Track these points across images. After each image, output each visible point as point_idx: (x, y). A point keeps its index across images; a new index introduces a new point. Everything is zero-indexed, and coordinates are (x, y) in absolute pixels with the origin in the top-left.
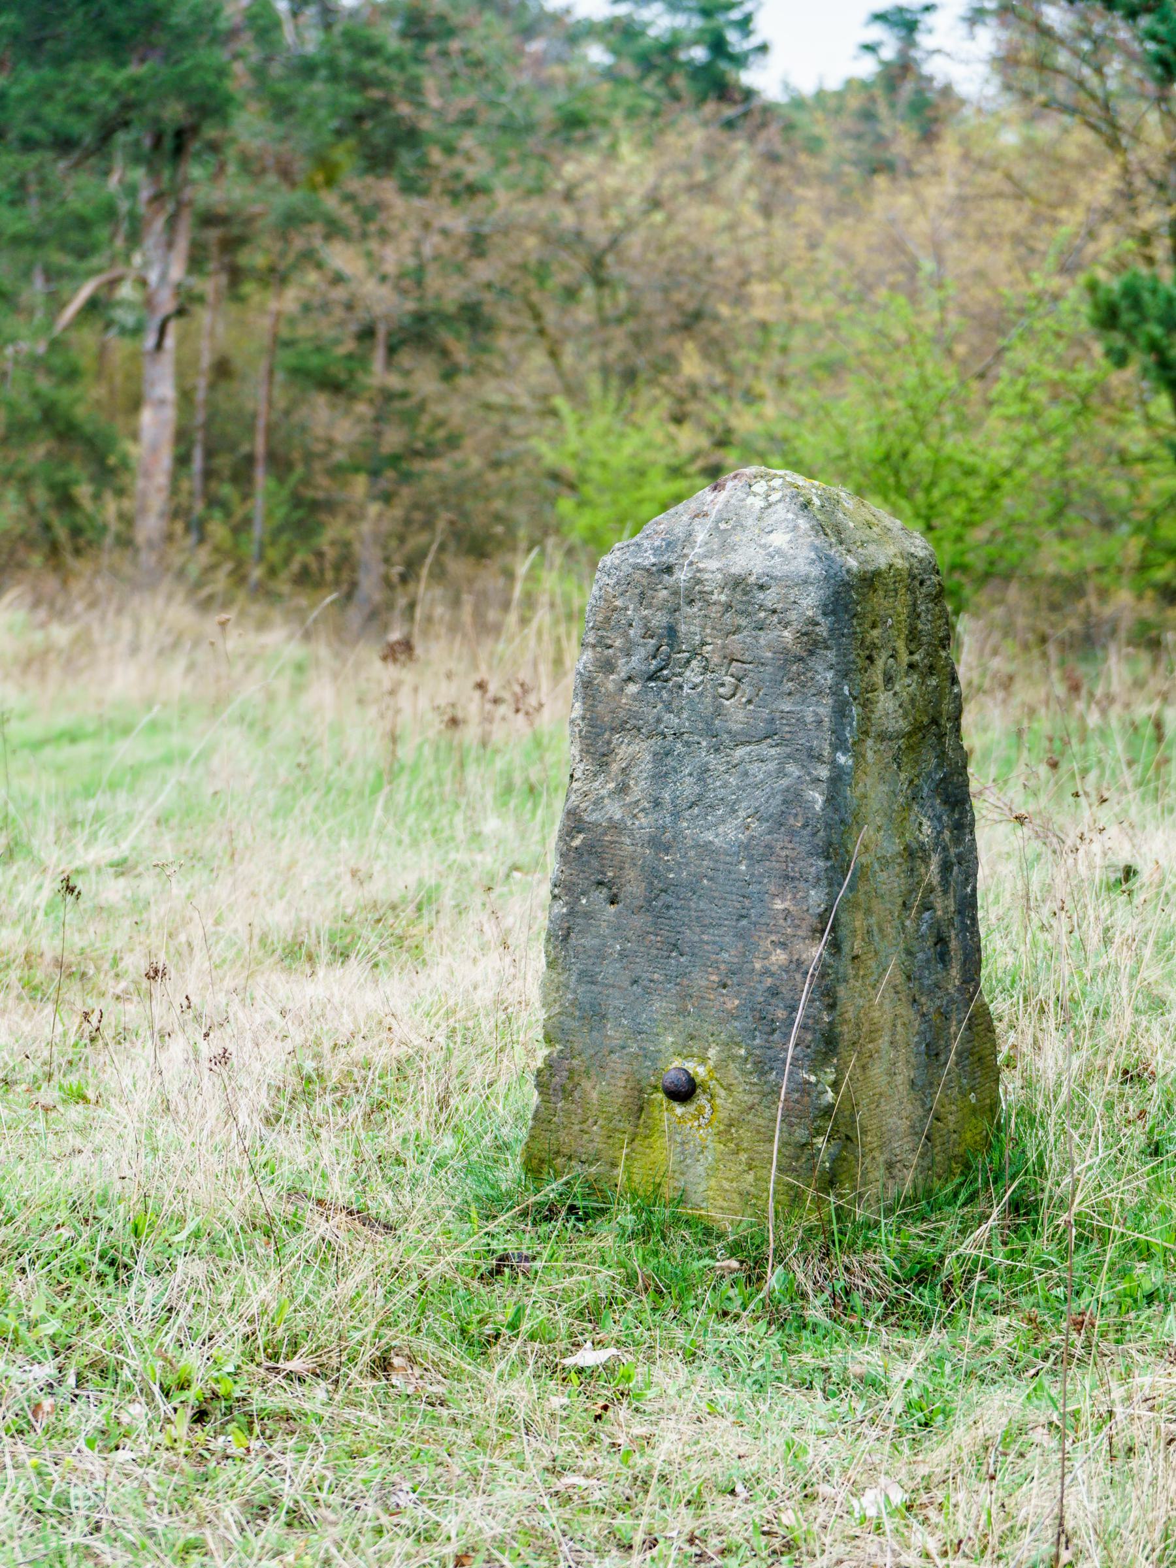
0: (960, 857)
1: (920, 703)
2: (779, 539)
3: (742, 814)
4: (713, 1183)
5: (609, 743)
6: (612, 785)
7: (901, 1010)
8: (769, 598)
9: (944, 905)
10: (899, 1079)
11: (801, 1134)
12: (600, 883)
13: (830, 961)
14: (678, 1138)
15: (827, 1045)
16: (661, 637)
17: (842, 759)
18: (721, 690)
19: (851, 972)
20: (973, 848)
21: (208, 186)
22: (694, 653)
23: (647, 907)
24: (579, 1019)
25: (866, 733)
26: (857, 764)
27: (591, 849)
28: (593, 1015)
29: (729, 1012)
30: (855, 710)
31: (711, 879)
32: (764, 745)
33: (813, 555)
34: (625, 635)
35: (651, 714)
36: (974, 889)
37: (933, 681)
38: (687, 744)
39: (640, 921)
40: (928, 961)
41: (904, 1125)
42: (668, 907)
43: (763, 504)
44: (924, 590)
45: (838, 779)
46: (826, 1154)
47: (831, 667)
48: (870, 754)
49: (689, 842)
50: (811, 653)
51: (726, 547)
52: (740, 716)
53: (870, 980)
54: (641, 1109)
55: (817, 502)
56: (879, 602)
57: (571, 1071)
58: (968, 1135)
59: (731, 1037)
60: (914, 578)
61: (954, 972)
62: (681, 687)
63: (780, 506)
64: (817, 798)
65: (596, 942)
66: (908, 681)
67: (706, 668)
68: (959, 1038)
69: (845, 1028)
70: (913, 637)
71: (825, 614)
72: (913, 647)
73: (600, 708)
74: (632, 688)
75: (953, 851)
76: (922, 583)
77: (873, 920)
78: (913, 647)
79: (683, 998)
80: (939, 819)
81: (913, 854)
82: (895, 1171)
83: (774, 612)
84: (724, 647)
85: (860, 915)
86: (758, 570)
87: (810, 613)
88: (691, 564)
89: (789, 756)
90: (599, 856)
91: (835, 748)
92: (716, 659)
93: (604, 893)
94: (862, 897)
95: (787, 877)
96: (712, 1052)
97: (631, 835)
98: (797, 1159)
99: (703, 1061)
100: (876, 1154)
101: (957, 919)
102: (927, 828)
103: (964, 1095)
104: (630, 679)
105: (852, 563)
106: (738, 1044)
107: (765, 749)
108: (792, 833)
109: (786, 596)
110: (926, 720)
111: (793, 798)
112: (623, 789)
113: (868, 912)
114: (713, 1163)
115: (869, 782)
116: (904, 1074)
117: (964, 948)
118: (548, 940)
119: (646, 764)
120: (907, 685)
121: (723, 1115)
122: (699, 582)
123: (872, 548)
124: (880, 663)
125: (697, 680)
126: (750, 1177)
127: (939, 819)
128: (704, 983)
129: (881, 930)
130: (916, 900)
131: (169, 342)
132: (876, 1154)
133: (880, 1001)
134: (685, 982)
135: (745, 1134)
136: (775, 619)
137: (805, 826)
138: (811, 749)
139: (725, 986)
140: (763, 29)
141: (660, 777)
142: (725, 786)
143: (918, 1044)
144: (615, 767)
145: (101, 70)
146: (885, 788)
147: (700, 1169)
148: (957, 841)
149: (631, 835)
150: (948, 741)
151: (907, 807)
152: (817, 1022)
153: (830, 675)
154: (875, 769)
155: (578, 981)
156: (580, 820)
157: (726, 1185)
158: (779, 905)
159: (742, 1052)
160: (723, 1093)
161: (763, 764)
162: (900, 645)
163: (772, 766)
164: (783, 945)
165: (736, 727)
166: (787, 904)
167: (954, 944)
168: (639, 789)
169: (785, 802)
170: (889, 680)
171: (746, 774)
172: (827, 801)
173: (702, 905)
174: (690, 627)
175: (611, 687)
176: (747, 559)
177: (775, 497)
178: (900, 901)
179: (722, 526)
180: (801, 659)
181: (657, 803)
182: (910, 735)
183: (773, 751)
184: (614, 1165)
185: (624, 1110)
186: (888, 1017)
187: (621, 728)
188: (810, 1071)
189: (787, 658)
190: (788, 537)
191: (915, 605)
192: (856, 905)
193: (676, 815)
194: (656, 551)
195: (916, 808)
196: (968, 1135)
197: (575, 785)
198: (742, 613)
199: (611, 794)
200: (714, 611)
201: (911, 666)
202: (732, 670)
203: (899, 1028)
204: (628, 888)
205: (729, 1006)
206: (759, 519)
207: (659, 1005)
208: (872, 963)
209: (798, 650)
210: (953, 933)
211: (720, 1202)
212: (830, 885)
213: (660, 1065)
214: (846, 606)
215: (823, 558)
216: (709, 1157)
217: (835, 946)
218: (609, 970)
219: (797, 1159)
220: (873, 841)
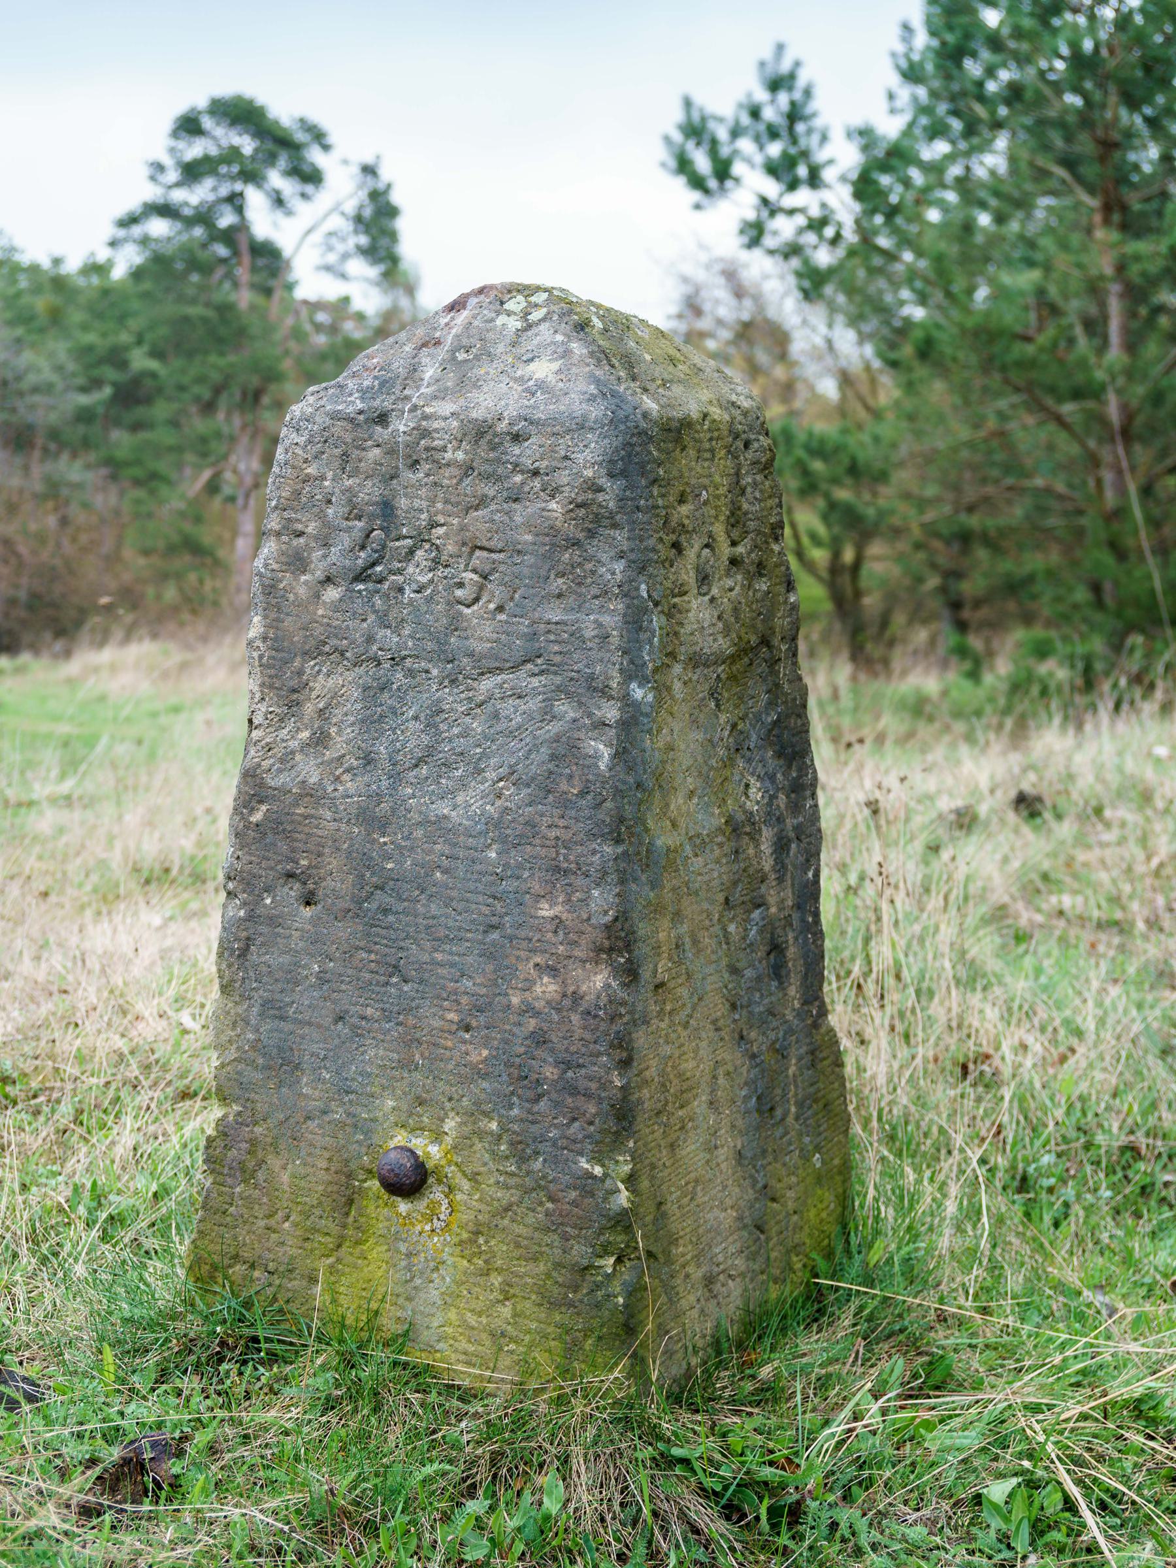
0: (798, 829)
1: (746, 614)
2: (543, 369)
3: (491, 775)
4: (452, 1315)
5: (300, 673)
6: (305, 735)
7: (725, 1055)
8: (528, 453)
9: (779, 898)
10: (722, 1153)
11: (579, 1252)
12: (290, 875)
13: (622, 994)
14: (403, 1247)
16: (372, 517)
17: (638, 693)
18: (459, 593)
19: (654, 1008)
20: (815, 817)
22: (420, 539)
23: (355, 911)
24: (265, 1060)
25: (672, 655)
26: (659, 700)
27: (276, 826)
28: (282, 1063)
29: (474, 1067)
30: (657, 621)
31: (445, 872)
32: (522, 674)
33: (592, 389)
34: (321, 516)
35: (359, 630)
36: (817, 874)
37: (762, 585)
38: (411, 673)
39: (344, 931)
40: (759, 979)
41: (727, 1218)
42: (386, 911)
43: (519, 325)
44: (750, 455)
45: (632, 723)
47: (621, 556)
48: (677, 686)
49: (415, 817)
50: (592, 534)
51: (465, 383)
52: (487, 629)
53: (682, 1016)
54: (350, 1202)
55: (598, 323)
56: (687, 465)
57: (253, 1142)
58: (812, 1213)
59: (477, 1103)
60: (737, 437)
61: (792, 991)
62: (401, 590)
63: (543, 327)
64: (602, 751)
65: (286, 959)
66: (730, 583)
67: (436, 562)
68: (796, 1082)
69: (646, 1093)
70: (736, 519)
71: (611, 475)
72: (735, 534)
73: (288, 622)
74: (332, 594)
75: (790, 822)
76: (747, 445)
77: (684, 928)
78: (735, 534)
79: (408, 1044)
80: (772, 778)
81: (738, 829)
82: (717, 1287)
83: (536, 473)
84: (463, 528)
85: (666, 923)
86: (511, 412)
87: (589, 473)
88: (415, 408)
89: (558, 689)
90: (288, 836)
91: (628, 676)
92: (451, 548)
93: (293, 891)
94: (668, 896)
95: (557, 869)
96: (450, 1125)
97: (333, 807)
98: (576, 1289)
99: (438, 1136)
100: (690, 1269)
101: (796, 916)
102: (755, 793)
103: (806, 1157)
104: (328, 580)
105: (650, 404)
106: (486, 1114)
107: (524, 679)
108: (565, 803)
109: (553, 449)
110: (754, 640)
111: (566, 751)
112: (320, 740)
113: (677, 916)
115: (677, 726)
116: (728, 1143)
117: (805, 956)
118: (220, 955)
119: (351, 706)
121: (466, 1217)
122: (426, 434)
123: (677, 390)
124: (691, 554)
125: (424, 579)
126: (506, 1311)
127: (772, 778)
128: (437, 1023)
129: (695, 942)
130: (743, 896)
131: (252, 502)
132: (690, 1269)
133: (696, 1055)
134: (411, 1021)
135: (499, 1247)
136: (537, 484)
137: (583, 793)
138: (592, 677)
139: (467, 1029)
141: (371, 722)
142: (464, 734)
143: (746, 1098)
144: (309, 709)
145: (213, 358)
146: (700, 736)
147: (434, 1294)
148: (795, 807)
149: (333, 807)
150: (783, 670)
151: (728, 763)
152: (603, 1087)
153: (619, 566)
154: (685, 708)
155: (261, 1014)
156: (262, 785)
157: (472, 1320)
158: (546, 911)
159: (494, 1126)
160: (466, 1185)
161: (521, 703)
162: (719, 529)
163: (534, 704)
164: (553, 971)
165: (480, 647)
166: (558, 910)
167: (792, 952)
168: (342, 741)
169: (553, 757)
170: (704, 579)
171: (496, 716)
172: (616, 756)
173: (434, 909)
174: (414, 499)
175: (302, 591)
177: (536, 315)
178: (721, 897)
179: (461, 356)
180: (577, 543)
181: (368, 760)
182: (733, 659)
183: (535, 682)
184: (313, 1280)
185: (327, 1202)
186: (707, 1066)
187: (316, 651)
188: (593, 1160)
189: (556, 541)
190: (555, 366)
191: (737, 474)
192: (658, 909)
193: (396, 777)
194: (364, 392)
195: (741, 764)
196: (812, 1213)
197: (256, 734)
198: (486, 477)
199: (305, 746)
200: (447, 477)
201: (734, 562)
202: (475, 562)
203: (721, 1081)
204: (329, 882)
205: (474, 1058)
206: (514, 344)
207: (374, 1054)
208: (684, 992)
209: (571, 530)
210: (791, 936)
211: (463, 1345)
212: (622, 882)
213: (376, 1140)
214: (642, 465)
215: (605, 393)
216: (445, 1279)
218: (303, 999)
219: (576, 1289)
220: (686, 817)
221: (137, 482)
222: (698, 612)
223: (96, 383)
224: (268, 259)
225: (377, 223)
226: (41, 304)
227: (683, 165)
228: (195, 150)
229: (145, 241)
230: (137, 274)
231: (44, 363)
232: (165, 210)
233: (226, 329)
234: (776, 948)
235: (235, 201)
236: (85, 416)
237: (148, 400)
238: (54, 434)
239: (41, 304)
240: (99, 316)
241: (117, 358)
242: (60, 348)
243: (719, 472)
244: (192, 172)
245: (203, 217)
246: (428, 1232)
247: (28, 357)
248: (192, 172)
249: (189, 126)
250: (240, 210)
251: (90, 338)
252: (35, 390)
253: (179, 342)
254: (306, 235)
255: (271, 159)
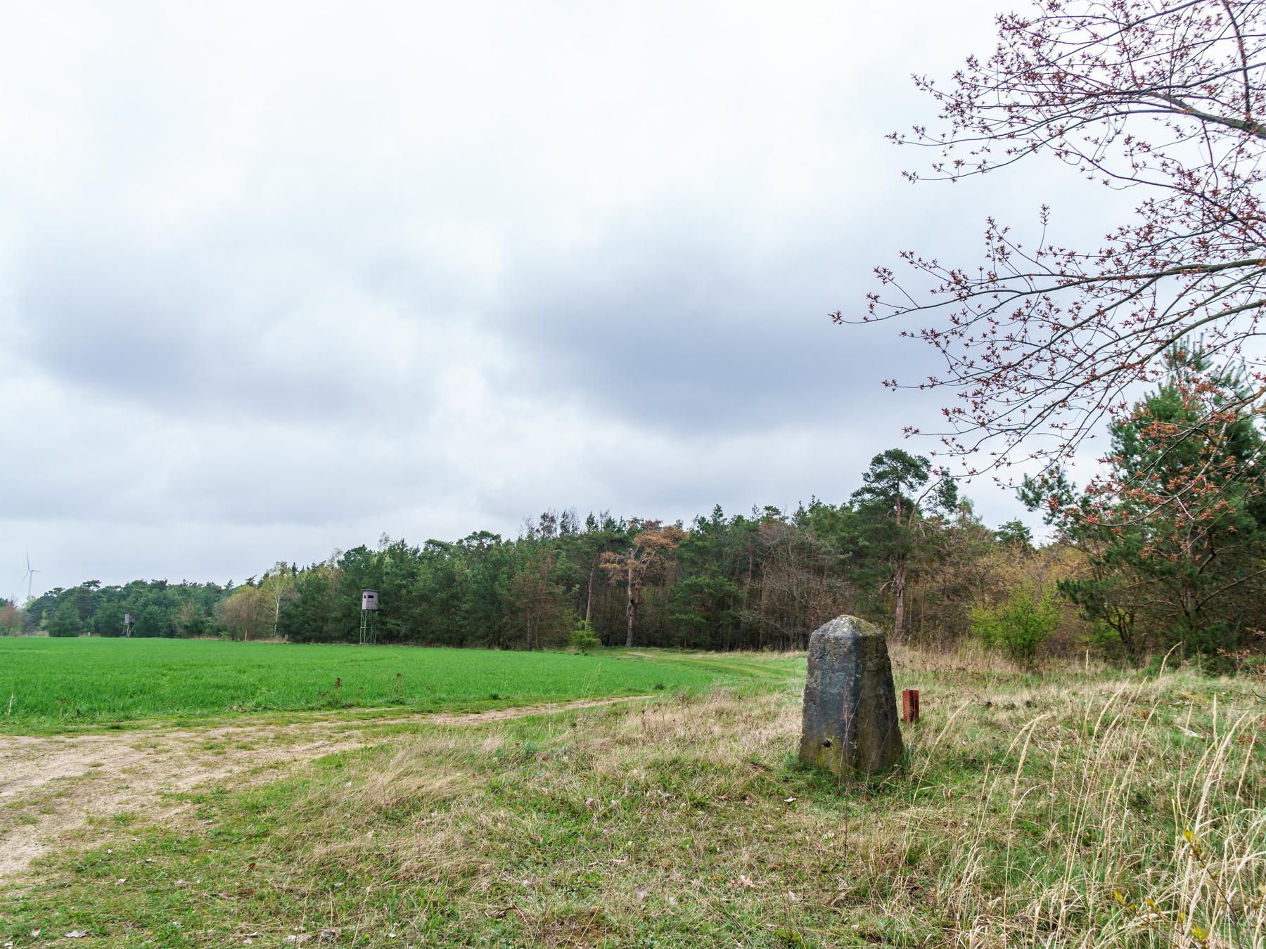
15: (855, 736)
21: (909, 564)
24: (808, 728)
45: (856, 680)
46: (857, 761)
70: (877, 650)
114: (834, 760)
116: (875, 744)
120: (875, 661)
133: (868, 726)
140: (1032, 533)
176: (838, 634)
189: (846, 654)
217: (856, 715)
220: (867, 693)
221: (861, 586)
222: (869, 664)
223: (846, 551)
224: (908, 506)
225: (948, 493)
226: (826, 522)
227: (1024, 496)
228: (880, 469)
229: (863, 500)
230: (859, 512)
231: (828, 543)
232: (869, 490)
233: (892, 532)
234: (886, 715)
235: (895, 487)
236: (842, 562)
237: (865, 556)
238: (831, 569)
239: (826, 522)
240: (847, 526)
241: (853, 541)
242: (834, 538)
243: (874, 643)
244: (879, 477)
245: (883, 492)
246: (830, 753)
247: (822, 541)
248: (879, 477)
249: (878, 461)
250: (897, 490)
251: (844, 534)
252: (825, 553)
253: (874, 535)
254: (922, 495)
255: (908, 471)
